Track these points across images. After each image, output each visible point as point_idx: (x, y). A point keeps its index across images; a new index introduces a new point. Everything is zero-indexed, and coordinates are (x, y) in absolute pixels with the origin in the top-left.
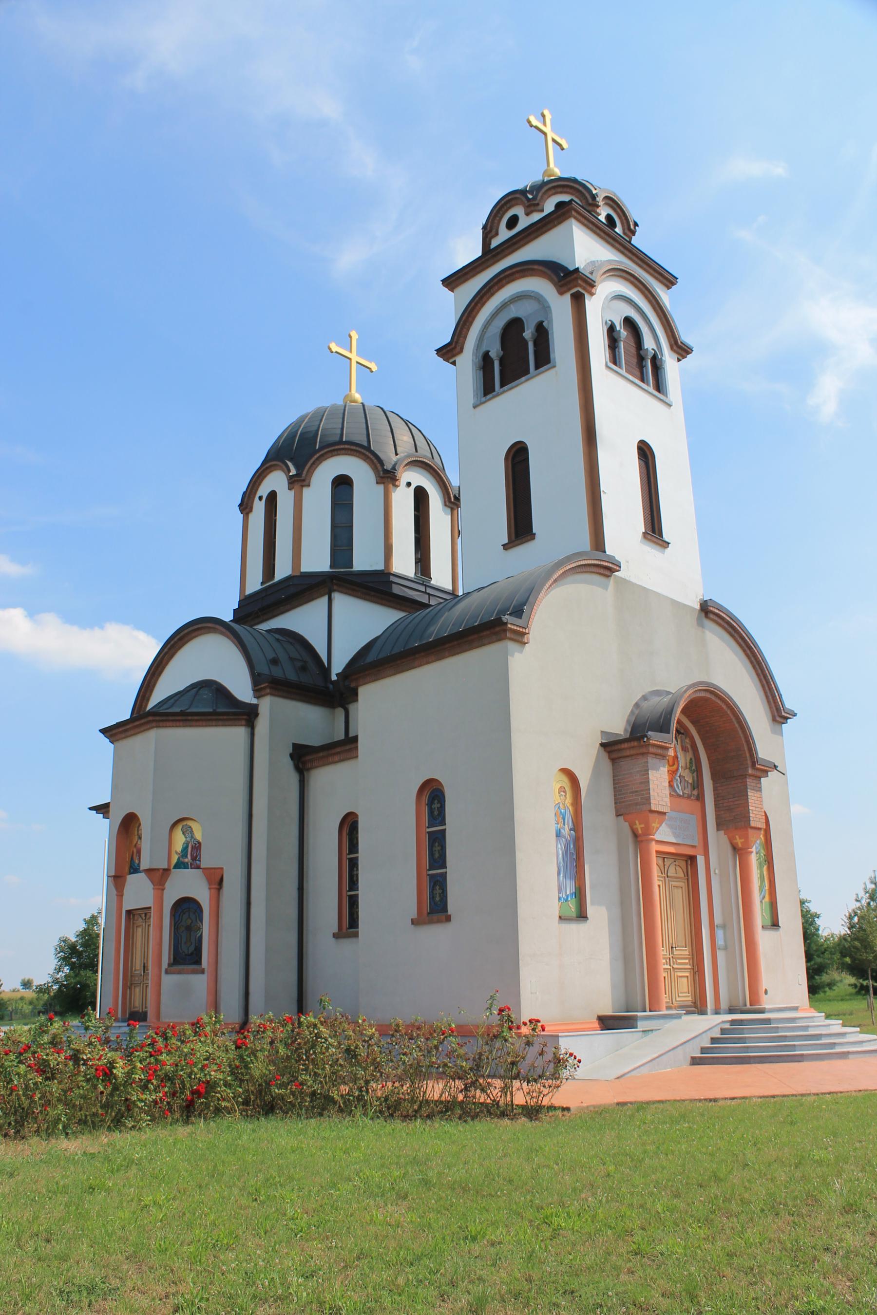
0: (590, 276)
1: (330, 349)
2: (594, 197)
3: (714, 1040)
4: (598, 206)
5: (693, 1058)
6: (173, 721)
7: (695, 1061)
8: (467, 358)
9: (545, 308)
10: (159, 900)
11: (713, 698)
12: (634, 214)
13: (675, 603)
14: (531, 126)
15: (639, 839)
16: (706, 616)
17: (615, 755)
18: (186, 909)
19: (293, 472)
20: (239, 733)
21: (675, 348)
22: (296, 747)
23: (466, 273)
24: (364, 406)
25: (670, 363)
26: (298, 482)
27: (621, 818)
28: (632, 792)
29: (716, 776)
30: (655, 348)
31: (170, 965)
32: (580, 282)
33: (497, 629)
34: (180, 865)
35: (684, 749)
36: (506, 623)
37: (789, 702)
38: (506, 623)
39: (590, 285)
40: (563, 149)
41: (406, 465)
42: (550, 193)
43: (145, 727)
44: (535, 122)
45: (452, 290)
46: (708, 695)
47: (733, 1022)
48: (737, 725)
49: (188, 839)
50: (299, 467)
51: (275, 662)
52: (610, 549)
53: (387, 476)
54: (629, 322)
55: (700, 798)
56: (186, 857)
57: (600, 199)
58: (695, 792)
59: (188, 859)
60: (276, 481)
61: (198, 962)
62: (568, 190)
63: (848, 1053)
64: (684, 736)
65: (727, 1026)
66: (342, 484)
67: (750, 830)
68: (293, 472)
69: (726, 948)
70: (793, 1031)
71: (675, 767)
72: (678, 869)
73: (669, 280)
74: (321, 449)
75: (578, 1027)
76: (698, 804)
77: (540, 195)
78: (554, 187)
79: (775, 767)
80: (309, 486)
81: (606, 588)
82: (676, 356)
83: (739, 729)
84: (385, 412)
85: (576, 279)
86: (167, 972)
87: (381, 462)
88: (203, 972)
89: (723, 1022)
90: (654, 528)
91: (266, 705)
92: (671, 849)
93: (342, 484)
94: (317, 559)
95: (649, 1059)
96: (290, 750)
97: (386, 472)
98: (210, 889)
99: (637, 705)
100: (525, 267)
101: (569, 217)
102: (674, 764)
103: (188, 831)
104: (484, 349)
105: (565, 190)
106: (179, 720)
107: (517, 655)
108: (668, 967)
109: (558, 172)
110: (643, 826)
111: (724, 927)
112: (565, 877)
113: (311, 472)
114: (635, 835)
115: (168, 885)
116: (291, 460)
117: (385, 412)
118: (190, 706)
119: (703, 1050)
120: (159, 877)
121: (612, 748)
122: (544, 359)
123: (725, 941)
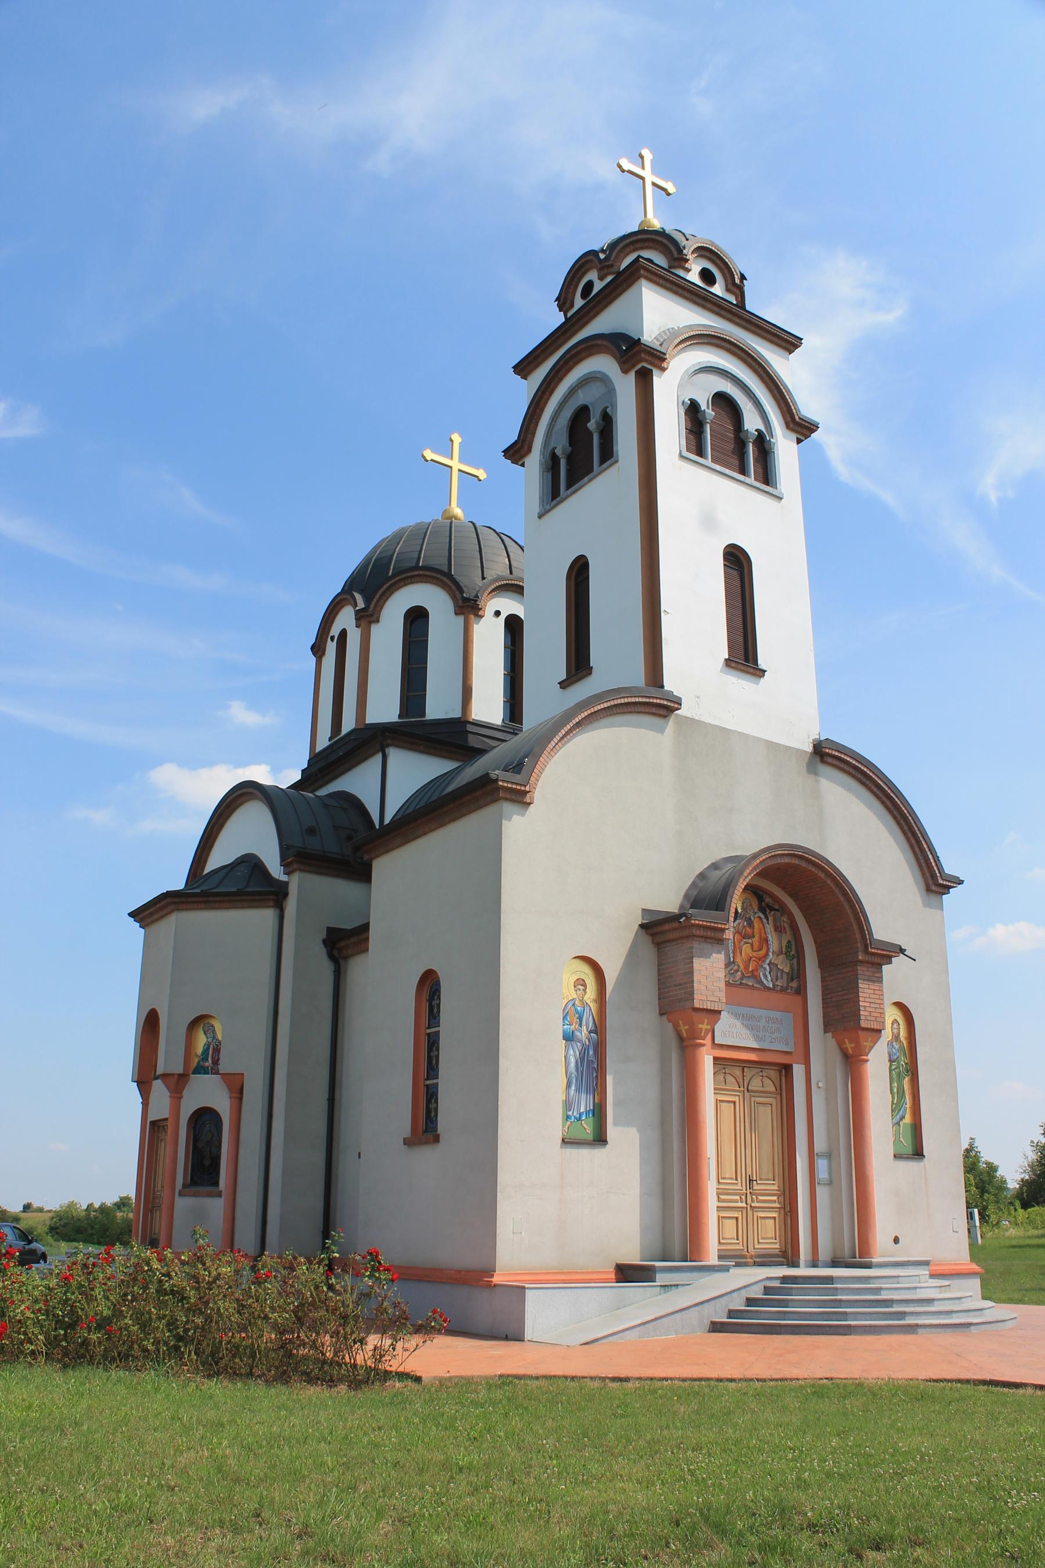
0: (659, 348)
1: (424, 457)
2: (680, 250)
3: (750, 1302)
4: (687, 261)
5: (713, 1323)
6: (193, 902)
7: (716, 1327)
8: (535, 459)
9: (611, 391)
10: (176, 1109)
11: (803, 864)
12: (740, 264)
13: (772, 746)
14: (623, 171)
15: (685, 1044)
16: (823, 761)
17: (659, 939)
18: (205, 1120)
19: (361, 605)
20: (266, 916)
21: (791, 426)
22: (330, 931)
23: (537, 357)
24: (474, 524)
25: (785, 448)
26: (367, 618)
27: (665, 1017)
28: (675, 986)
29: (825, 963)
30: (763, 429)
31: (184, 1186)
32: (643, 355)
33: (489, 788)
34: (200, 1070)
35: (778, 929)
36: (497, 780)
37: (950, 866)
38: (497, 780)
39: (658, 358)
40: (669, 194)
41: (493, 590)
42: (628, 250)
43: (161, 914)
44: (626, 165)
45: (525, 377)
46: (796, 861)
47: (785, 1279)
48: (842, 899)
49: (210, 1040)
50: (368, 600)
51: (311, 831)
52: (670, 683)
53: (468, 607)
54: (721, 399)
55: (801, 991)
56: (207, 1060)
57: (688, 252)
58: (794, 984)
59: (209, 1063)
60: (346, 619)
61: (216, 1183)
62: (650, 244)
63: (917, 1325)
64: (778, 914)
65: (776, 1284)
66: (417, 618)
67: (860, 1033)
68: (361, 605)
69: (830, 1183)
70: (859, 1294)
71: (763, 952)
72: (767, 1082)
73: (789, 343)
74: (394, 575)
75: (595, 1276)
76: (798, 999)
77: (614, 254)
78: (632, 243)
79: (902, 951)
80: (378, 621)
81: (662, 731)
82: (794, 436)
83: (845, 904)
84: (476, 529)
85: (639, 352)
86: (181, 1194)
87: (462, 591)
88: (219, 1195)
89: (768, 1279)
90: (744, 654)
91: (295, 882)
92: (752, 1057)
93: (417, 618)
94: (384, 707)
95: (639, 1322)
96: (324, 935)
97: (467, 600)
98: (231, 1098)
99: (702, 876)
100: (590, 344)
101: (638, 278)
102: (760, 949)
103: (210, 1031)
104: (552, 445)
105: (636, 246)
106: (198, 902)
107: (516, 818)
108: (744, 1205)
109: (656, 224)
110: (687, 1027)
111: (828, 1156)
112: (578, 1090)
113: (379, 606)
114: (681, 1039)
115: (185, 1093)
116: (361, 592)
117: (476, 529)
118: (246, 887)
119: (731, 1313)
120: (177, 1083)
121: (660, 931)
122: (608, 454)
123: (830, 1173)
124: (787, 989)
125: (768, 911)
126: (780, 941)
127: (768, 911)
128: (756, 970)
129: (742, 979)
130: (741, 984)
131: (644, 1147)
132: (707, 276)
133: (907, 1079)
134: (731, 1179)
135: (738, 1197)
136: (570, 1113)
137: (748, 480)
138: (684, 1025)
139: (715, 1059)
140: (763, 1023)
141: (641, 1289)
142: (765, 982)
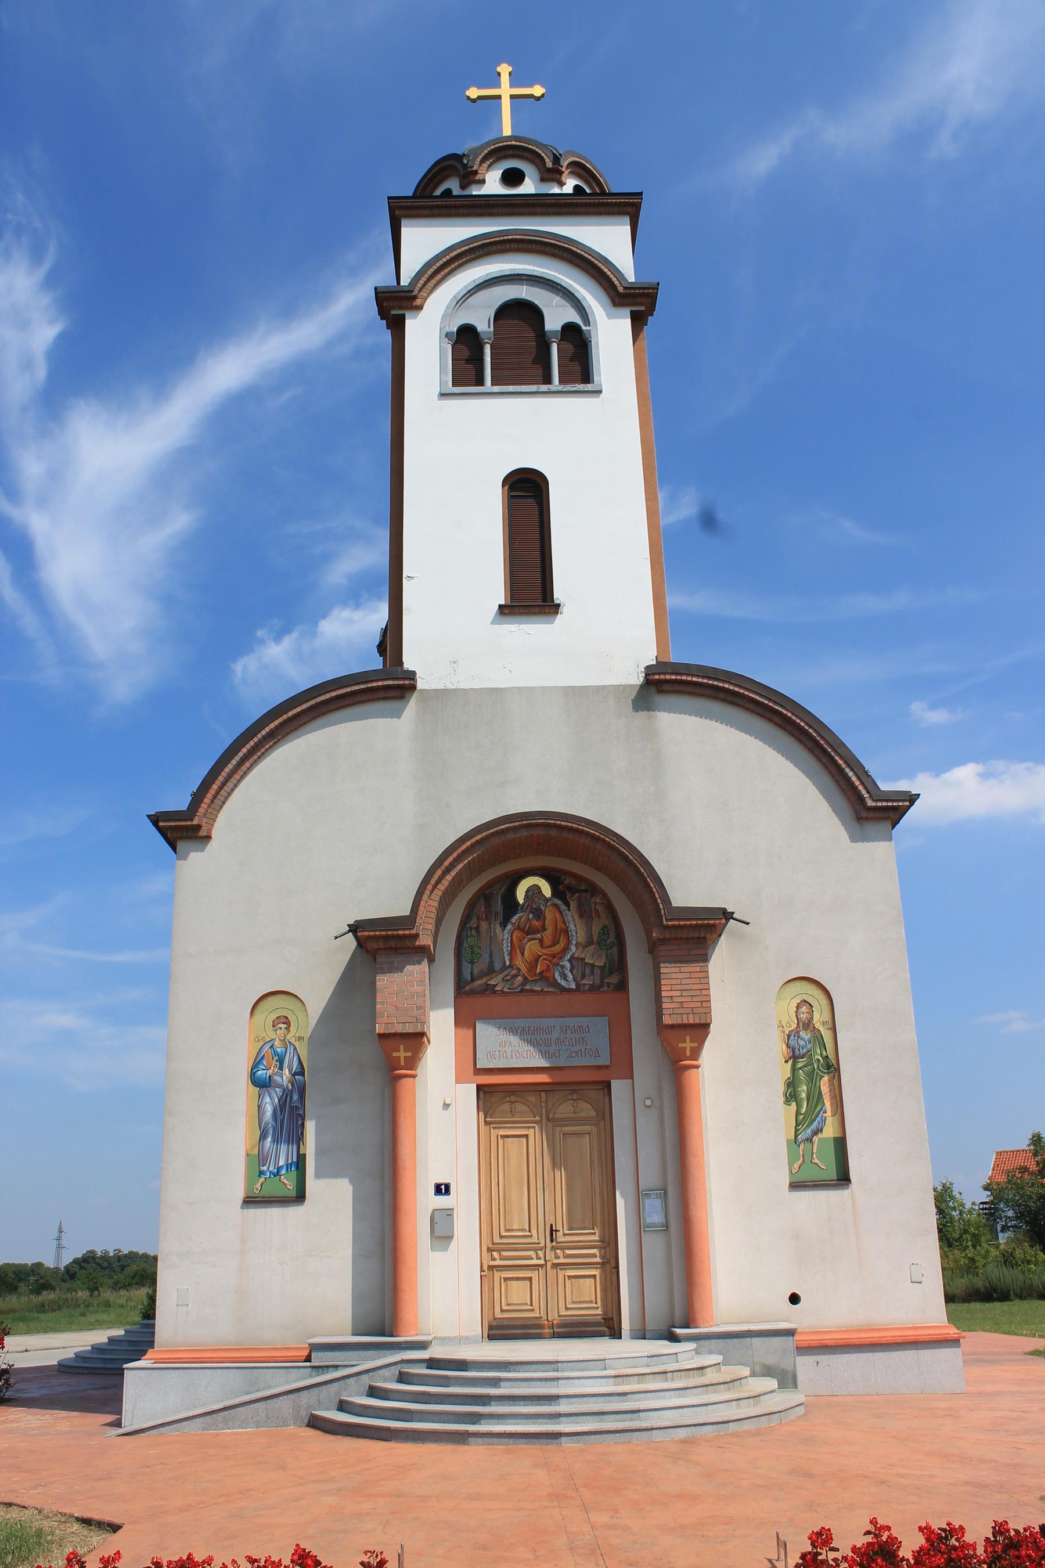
4: (476, 173)
16: (660, 691)
35: (584, 914)
58: (614, 979)
71: (558, 948)
79: (727, 915)
92: (543, 1078)
102: (555, 943)
108: (542, 1262)
112: (276, 1140)
124: (602, 985)
126: (589, 929)
129: (524, 984)
130: (522, 991)
131: (358, 1200)
132: (512, 178)
133: (826, 1078)
134: (523, 1230)
135: (531, 1253)
136: (265, 1168)
137: (552, 387)
138: (405, 1051)
139: (479, 1088)
141: (284, 1370)
142: (563, 983)
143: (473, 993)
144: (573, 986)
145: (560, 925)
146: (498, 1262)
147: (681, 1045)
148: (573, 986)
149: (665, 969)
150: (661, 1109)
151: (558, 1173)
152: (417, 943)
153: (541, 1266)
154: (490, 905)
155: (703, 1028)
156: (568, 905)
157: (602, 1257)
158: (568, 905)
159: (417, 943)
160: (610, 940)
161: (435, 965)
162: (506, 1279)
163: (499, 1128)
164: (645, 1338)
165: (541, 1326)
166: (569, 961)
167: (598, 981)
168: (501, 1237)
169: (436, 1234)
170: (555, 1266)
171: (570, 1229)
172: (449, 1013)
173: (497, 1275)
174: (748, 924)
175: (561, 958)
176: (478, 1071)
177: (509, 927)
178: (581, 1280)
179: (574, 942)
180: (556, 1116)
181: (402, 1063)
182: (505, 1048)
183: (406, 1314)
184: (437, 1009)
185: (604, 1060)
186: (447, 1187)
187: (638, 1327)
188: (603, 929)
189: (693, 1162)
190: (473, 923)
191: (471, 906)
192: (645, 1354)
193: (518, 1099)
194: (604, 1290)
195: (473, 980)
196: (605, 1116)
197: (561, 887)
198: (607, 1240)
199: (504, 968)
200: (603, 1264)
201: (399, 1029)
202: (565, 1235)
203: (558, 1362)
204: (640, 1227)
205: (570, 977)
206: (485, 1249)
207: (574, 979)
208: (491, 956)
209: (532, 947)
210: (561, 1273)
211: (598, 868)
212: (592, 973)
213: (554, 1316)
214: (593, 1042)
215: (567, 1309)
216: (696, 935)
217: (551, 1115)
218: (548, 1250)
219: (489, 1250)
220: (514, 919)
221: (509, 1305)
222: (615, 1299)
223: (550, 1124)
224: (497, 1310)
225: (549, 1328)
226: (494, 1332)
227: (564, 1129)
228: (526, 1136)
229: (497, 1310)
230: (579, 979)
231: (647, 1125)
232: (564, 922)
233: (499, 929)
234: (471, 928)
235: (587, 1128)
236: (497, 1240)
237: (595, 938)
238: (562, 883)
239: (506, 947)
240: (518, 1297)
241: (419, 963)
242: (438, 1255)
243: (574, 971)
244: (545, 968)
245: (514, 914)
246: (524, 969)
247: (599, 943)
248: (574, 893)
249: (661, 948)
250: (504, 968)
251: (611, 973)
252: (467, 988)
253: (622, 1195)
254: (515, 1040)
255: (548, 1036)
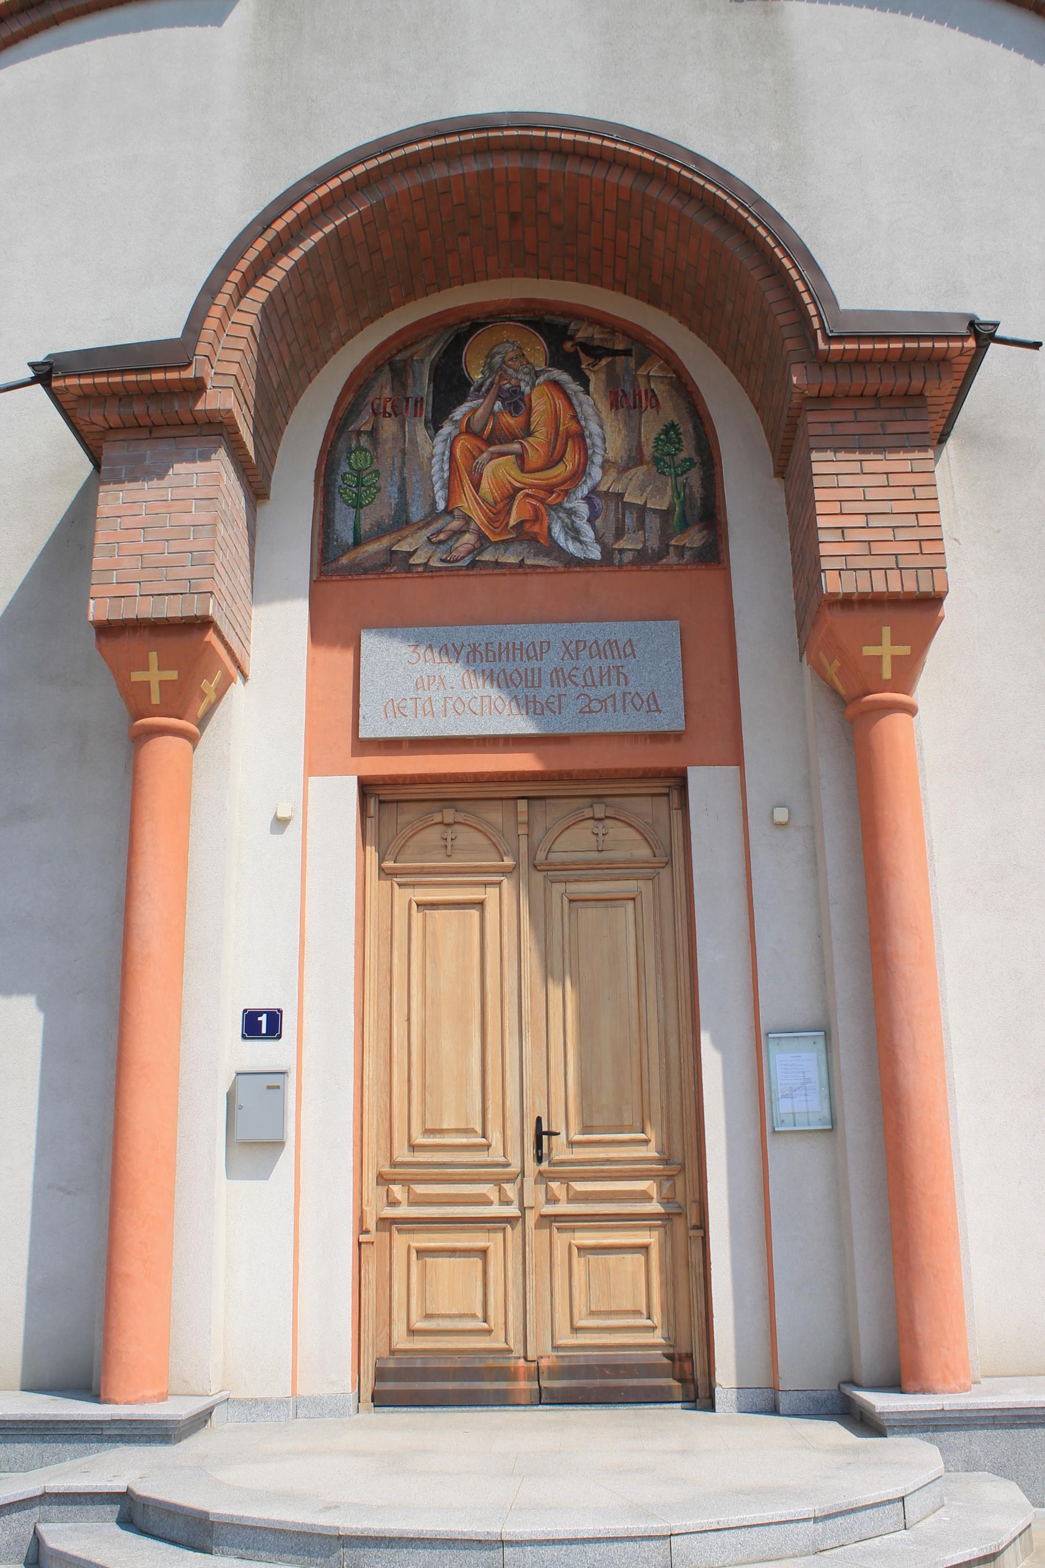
58: (694, 538)
71: (560, 471)
79: (983, 334)
92: (524, 762)
108: (513, 1211)
124: (663, 551)
125: (585, 362)
126: (634, 432)
127: (585, 362)
128: (537, 518)
130: (473, 564)
134: (467, 1131)
135: (487, 1189)
139: (367, 788)
140: (553, 659)
142: (572, 547)
143: (359, 570)
144: (595, 554)
145: (566, 424)
146: (404, 1211)
147: (869, 651)
148: (595, 554)
149: (824, 465)
150: (814, 830)
151: (555, 992)
152: (200, 406)
153: (508, 1220)
154: (404, 386)
155: (928, 603)
156: (585, 383)
157: (665, 1201)
158: (585, 383)
159: (200, 406)
160: (683, 455)
161: (266, 510)
162: (421, 1253)
163: (414, 885)
164: (774, 1410)
165: (506, 1374)
166: (587, 499)
167: (654, 543)
168: (413, 1147)
169: (240, 1135)
170: (547, 1220)
171: (586, 1129)
172: (296, 612)
173: (401, 1241)
174: (1036, 345)
175: (567, 493)
176: (363, 746)
177: (447, 429)
178: (612, 1258)
179: (598, 459)
180: (554, 857)
181: (156, 699)
182: (431, 690)
183: (133, 1346)
184: (270, 600)
185: (670, 719)
186: (275, 1018)
187: (759, 1379)
188: (666, 432)
189: (905, 945)
190: (364, 421)
191: (358, 387)
192: (807, 1510)
193: (460, 817)
194: (670, 1283)
195: (357, 543)
196: (674, 857)
197: (568, 346)
198: (678, 1157)
199: (433, 515)
200: (667, 1218)
201: (146, 609)
202: (572, 1144)
203: (503, 1543)
204: (761, 1127)
205: (588, 533)
206: (370, 1177)
207: (598, 540)
208: (402, 490)
209: (498, 471)
210: (562, 1240)
211: (653, 298)
212: (641, 525)
213: (541, 1348)
214: (639, 678)
215: (575, 1330)
216: (901, 382)
217: (541, 856)
218: (529, 1182)
219: (382, 1179)
220: (458, 413)
221: (428, 1316)
222: (699, 1307)
223: (539, 877)
224: (399, 1330)
225: (529, 1378)
226: (390, 1386)
227: (574, 888)
228: (480, 904)
229: (399, 1330)
230: (609, 539)
231: (779, 869)
232: (575, 417)
233: (422, 434)
234: (359, 433)
235: (629, 886)
236: (402, 1154)
237: (648, 450)
238: (571, 338)
239: (439, 472)
240: (452, 1299)
241: (205, 457)
242: (245, 1187)
243: (598, 522)
244: (528, 515)
245: (460, 403)
246: (478, 517)
247: (656, 461)
248: (599, 358)
249: (811, 417)
250: (433, 515)
251: (685, 525)
252: (344, 561)
253: (717, 1043)
254: (454, 672)
255: (536, 665)
